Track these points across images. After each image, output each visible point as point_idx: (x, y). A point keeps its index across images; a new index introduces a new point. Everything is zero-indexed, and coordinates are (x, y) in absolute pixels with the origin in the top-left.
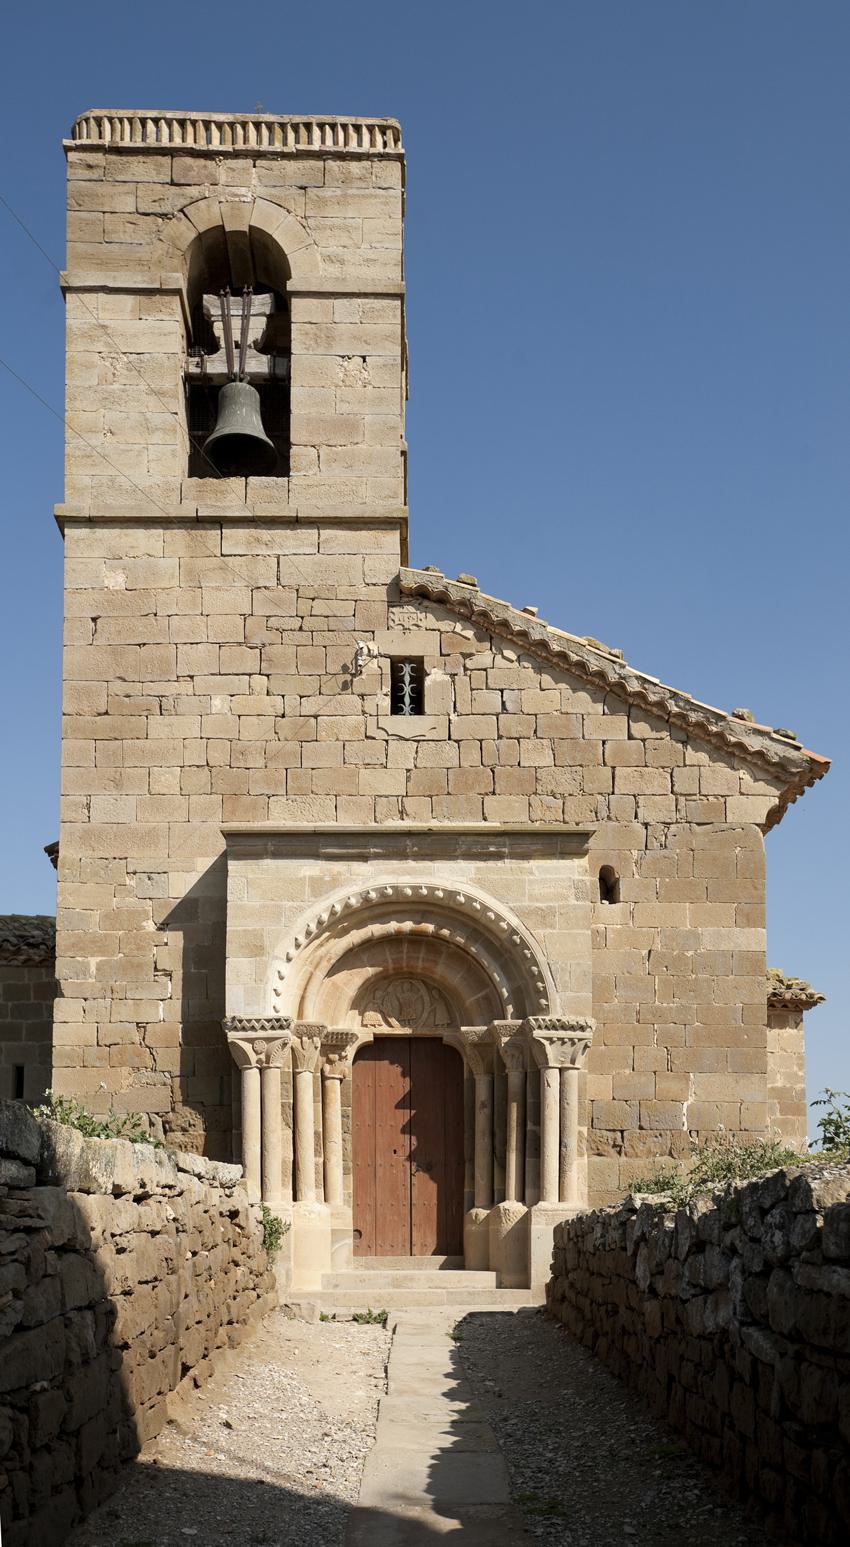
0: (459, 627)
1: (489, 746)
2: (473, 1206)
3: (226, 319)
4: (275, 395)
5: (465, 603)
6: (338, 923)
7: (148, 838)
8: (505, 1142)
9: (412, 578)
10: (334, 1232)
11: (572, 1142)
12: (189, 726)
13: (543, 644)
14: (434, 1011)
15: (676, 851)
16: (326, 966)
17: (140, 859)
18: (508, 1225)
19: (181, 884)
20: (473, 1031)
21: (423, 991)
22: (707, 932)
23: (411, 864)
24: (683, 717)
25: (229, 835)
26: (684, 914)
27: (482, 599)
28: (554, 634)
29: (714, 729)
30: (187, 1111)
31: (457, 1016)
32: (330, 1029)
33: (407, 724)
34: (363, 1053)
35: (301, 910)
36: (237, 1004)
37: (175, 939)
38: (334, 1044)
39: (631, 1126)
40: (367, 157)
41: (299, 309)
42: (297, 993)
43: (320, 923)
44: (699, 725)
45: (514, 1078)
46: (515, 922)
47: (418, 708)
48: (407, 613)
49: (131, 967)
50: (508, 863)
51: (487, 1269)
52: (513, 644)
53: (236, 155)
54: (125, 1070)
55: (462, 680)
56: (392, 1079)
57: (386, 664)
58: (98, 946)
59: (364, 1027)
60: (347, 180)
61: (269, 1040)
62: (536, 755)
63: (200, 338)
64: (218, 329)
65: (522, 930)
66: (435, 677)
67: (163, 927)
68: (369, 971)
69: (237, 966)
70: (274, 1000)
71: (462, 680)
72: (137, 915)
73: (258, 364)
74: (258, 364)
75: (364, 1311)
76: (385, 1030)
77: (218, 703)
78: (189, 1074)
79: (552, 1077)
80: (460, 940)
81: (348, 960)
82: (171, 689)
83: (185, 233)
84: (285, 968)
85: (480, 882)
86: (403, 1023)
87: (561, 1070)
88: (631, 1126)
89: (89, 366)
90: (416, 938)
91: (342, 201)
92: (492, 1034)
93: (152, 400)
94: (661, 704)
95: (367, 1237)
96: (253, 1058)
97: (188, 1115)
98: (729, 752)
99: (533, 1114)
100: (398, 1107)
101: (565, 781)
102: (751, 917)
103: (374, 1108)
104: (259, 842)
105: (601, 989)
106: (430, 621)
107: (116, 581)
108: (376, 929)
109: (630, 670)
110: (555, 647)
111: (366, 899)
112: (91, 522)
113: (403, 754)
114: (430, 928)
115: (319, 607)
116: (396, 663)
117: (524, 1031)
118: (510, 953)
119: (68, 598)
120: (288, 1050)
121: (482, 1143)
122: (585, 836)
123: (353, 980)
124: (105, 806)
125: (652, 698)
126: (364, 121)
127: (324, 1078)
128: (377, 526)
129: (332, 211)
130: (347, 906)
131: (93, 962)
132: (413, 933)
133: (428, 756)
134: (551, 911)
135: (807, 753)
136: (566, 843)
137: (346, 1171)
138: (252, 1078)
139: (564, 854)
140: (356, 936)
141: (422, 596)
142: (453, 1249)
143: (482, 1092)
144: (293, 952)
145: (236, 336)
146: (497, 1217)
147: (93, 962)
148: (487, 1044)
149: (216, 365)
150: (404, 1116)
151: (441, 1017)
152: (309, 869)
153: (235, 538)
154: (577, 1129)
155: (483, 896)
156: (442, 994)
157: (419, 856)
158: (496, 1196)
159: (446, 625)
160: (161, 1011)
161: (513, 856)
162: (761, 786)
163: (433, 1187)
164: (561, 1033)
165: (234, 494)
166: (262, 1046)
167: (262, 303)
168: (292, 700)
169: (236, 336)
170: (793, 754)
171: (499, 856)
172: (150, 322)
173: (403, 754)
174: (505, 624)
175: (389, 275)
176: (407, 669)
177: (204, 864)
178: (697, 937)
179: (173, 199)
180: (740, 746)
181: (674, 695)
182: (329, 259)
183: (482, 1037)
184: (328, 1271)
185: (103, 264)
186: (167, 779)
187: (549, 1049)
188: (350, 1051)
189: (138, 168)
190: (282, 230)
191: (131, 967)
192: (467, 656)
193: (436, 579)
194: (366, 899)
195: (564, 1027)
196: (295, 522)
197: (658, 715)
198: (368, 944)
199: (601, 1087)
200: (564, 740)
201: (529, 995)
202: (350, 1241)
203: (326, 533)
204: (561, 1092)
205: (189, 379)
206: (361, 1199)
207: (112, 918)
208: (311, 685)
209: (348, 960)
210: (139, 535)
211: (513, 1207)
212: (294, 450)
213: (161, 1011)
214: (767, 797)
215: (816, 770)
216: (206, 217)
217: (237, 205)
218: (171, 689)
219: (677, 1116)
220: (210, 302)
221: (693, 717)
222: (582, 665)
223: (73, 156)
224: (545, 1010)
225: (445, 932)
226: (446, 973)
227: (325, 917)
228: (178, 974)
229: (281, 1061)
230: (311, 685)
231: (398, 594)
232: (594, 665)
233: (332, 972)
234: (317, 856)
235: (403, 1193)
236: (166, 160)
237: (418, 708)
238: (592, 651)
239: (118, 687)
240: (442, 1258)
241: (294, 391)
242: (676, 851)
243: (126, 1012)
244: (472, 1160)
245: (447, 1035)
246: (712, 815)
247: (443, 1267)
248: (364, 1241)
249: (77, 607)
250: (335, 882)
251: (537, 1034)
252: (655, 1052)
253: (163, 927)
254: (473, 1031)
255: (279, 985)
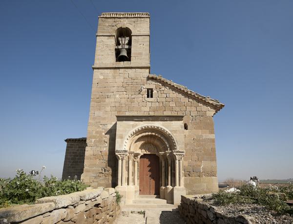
0: (159, 84)
1: (164, 103)
2: (161, 186)
3: (122, 41)
4: (129, 51)
5: (160, 80)
6: (137, 133)
7: (104, 119)
8: (168, 181)
9: (151, 76)
10: (135, 191)
11: (181, 174)
12: (112, 100)
13: (173, 86)
14: (154, 150)
15: (198, 121)
16: (135, 141)
17: (103, 122)
18: (169, 191)
19: (109, 127)
20: (162, 153)
21: (152, 146)
22: (204, 135)
23: (150, 122)
24: (198, 98)
25: (118, 117)
26: (200, 132)
27: (163, 79)
28: (175, 85)
29: (204, 100)
30: (109, 167)
31: (159, 150)
32: (135, 152)
33: (150, 99)
34: (142, 157)
35: (130, 130)
36: (117, 148)
37: (108, 136)
38: (136, 155)
39: (192, 171)
40: (144, 18)
41: (133, 38)
42: (129, 146)
43: (133, 133)
44: (201, 99)
45: (170, 162)
46: (170, 132)
47: (152, 97)
48: (150, 82)
49: (100, 141)
50: (168, 122)
51: (165, 199)
52: (168, 86)
53: (124, 18)
54: (98, 160)
55: (159, 92)
56: (147, 162)
57: (146, 90)
58: (94, 137)
59: (142, 152)
60: (141, 21)
61: (123, 154)
62: (172, 104)
63: (118, 43)
64: (121, 42)
65: (171, 134)
66: (155, 92)
67: (106, 134)
68: (143, 142)
69: (118, 140)
70: (124, 147)
71: (159, 92)
72: (101, 132)
73: (127, 47)
74: (127, 47)
75: (140, 211)
76: (145, 153)
77: (117, 96)
78: (109, 161)
79: (177, 162)
80: (159, 136)
81: (138, 140)
82: (110, 94)
83: (116, 28)
84: (127, 141)
85: (163, 125)
86: (149, 152)
87: (179, 160)
88: (192, 171)
89: (100, 46)
90: (151, 136)
91: (141, 23)
92: (165, 154)
93: (109, 51)
94: (194, 96)
95: (142, 191)
96: (120, 158)
97: (109, 168)
98: (206, 104)
99: (174, 169)
100: (148, 167)
101: (178, 109)
102: (212, 132)
103: (144, 168)
104: (122, 118)
105: (186, 145)
106: (154, 83)
107: (102, 77)
108: (144, 134)
109: (188, 90)
110: (176, 86)
111: (142, 128)
112: (98, 68)
113: (149, 104)
114: (154, 134)
115: (135, 81)
116: (148, 90)
117: (172, 153)
118: (169, 138)
119: (93, 80)
120: (127, 156)
121: (163, 174)
122: (183, 117)
123: (140, 143)
124: (97, 113)
125: (193, 95)
126: (144, 13)
127: (134, 162)
128: (160, 165)
129: (139, 25)
130: (139, 130)
131: (93, 140)
132: (151, 135)
133: (154, 105)
134: (177, 131)
135: (220, 103)
136: (179, 118)
137: (138, 179)
138: (120, 162)
139: (179, 120)
140: (140, 135)
141: (152, 79)
142: (158, 194)
143: (163, 164)
144: (128, 138)
145: (123, 43)
146: (167, 189)
147: (93, 140)
148: (164, 155)
149: (120, 47)
150: (149, 168)
151: (156, 151)
152: (132, 123)
153: (122, 71)
154: (182, 172)
155: (164, 128)
156: (156, 146)
157: (152, 121)
158: (166, 185)
159: (156, 84)
160: (105, 149)
161: (169, 121)
162: (212, 110)
163: (154, 182)
164: (179, 153)
165: (122, 64)
166: (122, 155)
167: (128, 38)
168: (130, 96)
169: (123, 43)
170: (218, 104)
171: (166, 121)
172: (110, 40)
173: (149, 104)
174: (167, 83)
175: (148, 33)
176: (150, 91)
177: (114, 123)
178: (202, 136)
179: (114, 24)
180: (208, 103)
181: (197, 94)
182: (138, 31)
183: (163, 154)
184: (134, 199)
185: (103, 32)
186: (108, 109)
187: (177, 156)
188: (139, 157)
189: (109, 20)
190: (131, 27)
191: (100, 141)
192: (160, 88)
193: (155, 76)
194: (142, 128)
195: (179, 152)
196: (131, 68)
197: (193, 98)
198: (142, 137)
199: (186, 163)
200: (178, 103)
201: (172, 146)
202: (138, 193)
203: (137, 70)
204: (179, 168)
205: (116, 49)
206: (141, 184)
207: (97, 132)
208: (133, 93)
209: (138, 140)
210: (106, 70)
211: (170, 187)
212: (132, 58)
213: (105, 149)
214: (213, 111)
215: (222, 106)
216: (119, 26)
217: (124, 24)
218: (110, 94)
219: (200, 169)
220: (120, 39)
221: (200, 98)
222: (180, 89)
223: (100, 19)
224: (176, 149)
225: (157, 135)
226: (157, 142)
227: (134, 132)
228: (108, 142)
229: (126, 158)
230: (133, 93)
231: (149, 78)
232: (182, 89)
233: (135, 143)
234: (133, 121)
235: (149, 183)
236: (113, 19)
237: (152, 97)
238: (182, 87)
239: (101, 94)
240: (156, 196)
241: (132, 49)
242: (198, 121)
243: (98, 149)
244: (161, 177)
245: (157, 154)
246: (203, 115)
247: (156, 198)
248: (141, 192)
249: (95, 81)
250: (136, 125)
251: (174, 153)
252: (195, 157)
253: (106, 134)
254: (162, 153)
255: (126, 144)
